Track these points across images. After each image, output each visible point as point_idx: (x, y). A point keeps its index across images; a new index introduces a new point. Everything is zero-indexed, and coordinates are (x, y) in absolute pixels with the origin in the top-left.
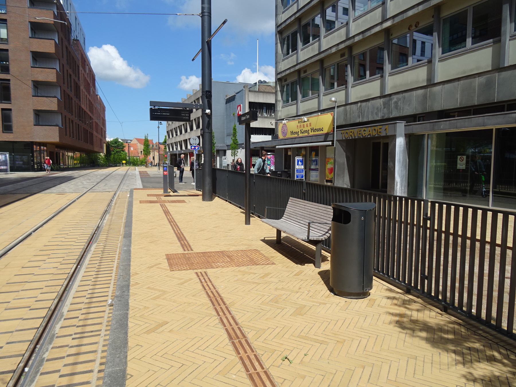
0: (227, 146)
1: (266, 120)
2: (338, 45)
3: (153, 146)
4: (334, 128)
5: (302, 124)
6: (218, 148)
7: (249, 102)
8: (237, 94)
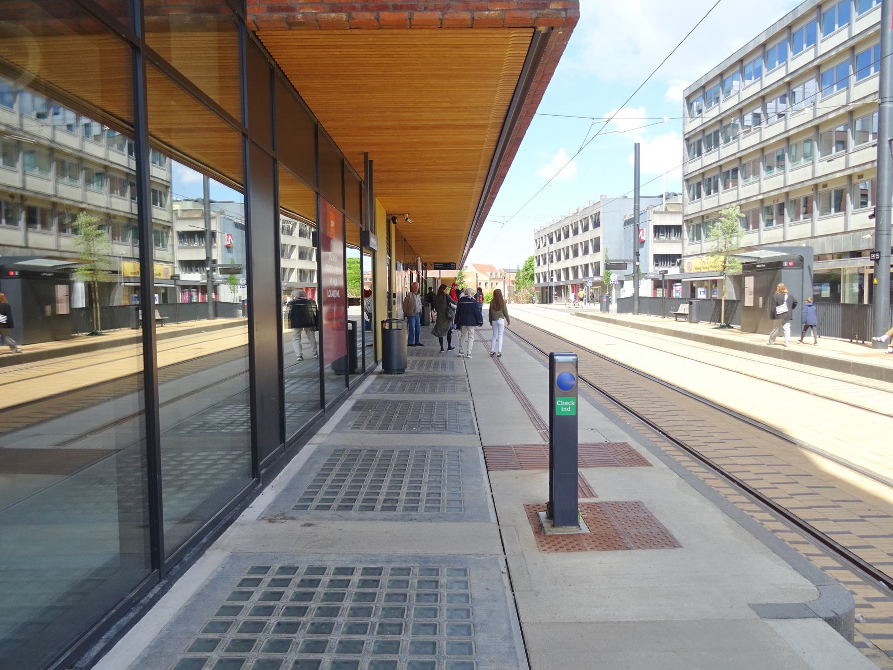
0: (625, 276)
1: (675, 244)
3: (496, 274)
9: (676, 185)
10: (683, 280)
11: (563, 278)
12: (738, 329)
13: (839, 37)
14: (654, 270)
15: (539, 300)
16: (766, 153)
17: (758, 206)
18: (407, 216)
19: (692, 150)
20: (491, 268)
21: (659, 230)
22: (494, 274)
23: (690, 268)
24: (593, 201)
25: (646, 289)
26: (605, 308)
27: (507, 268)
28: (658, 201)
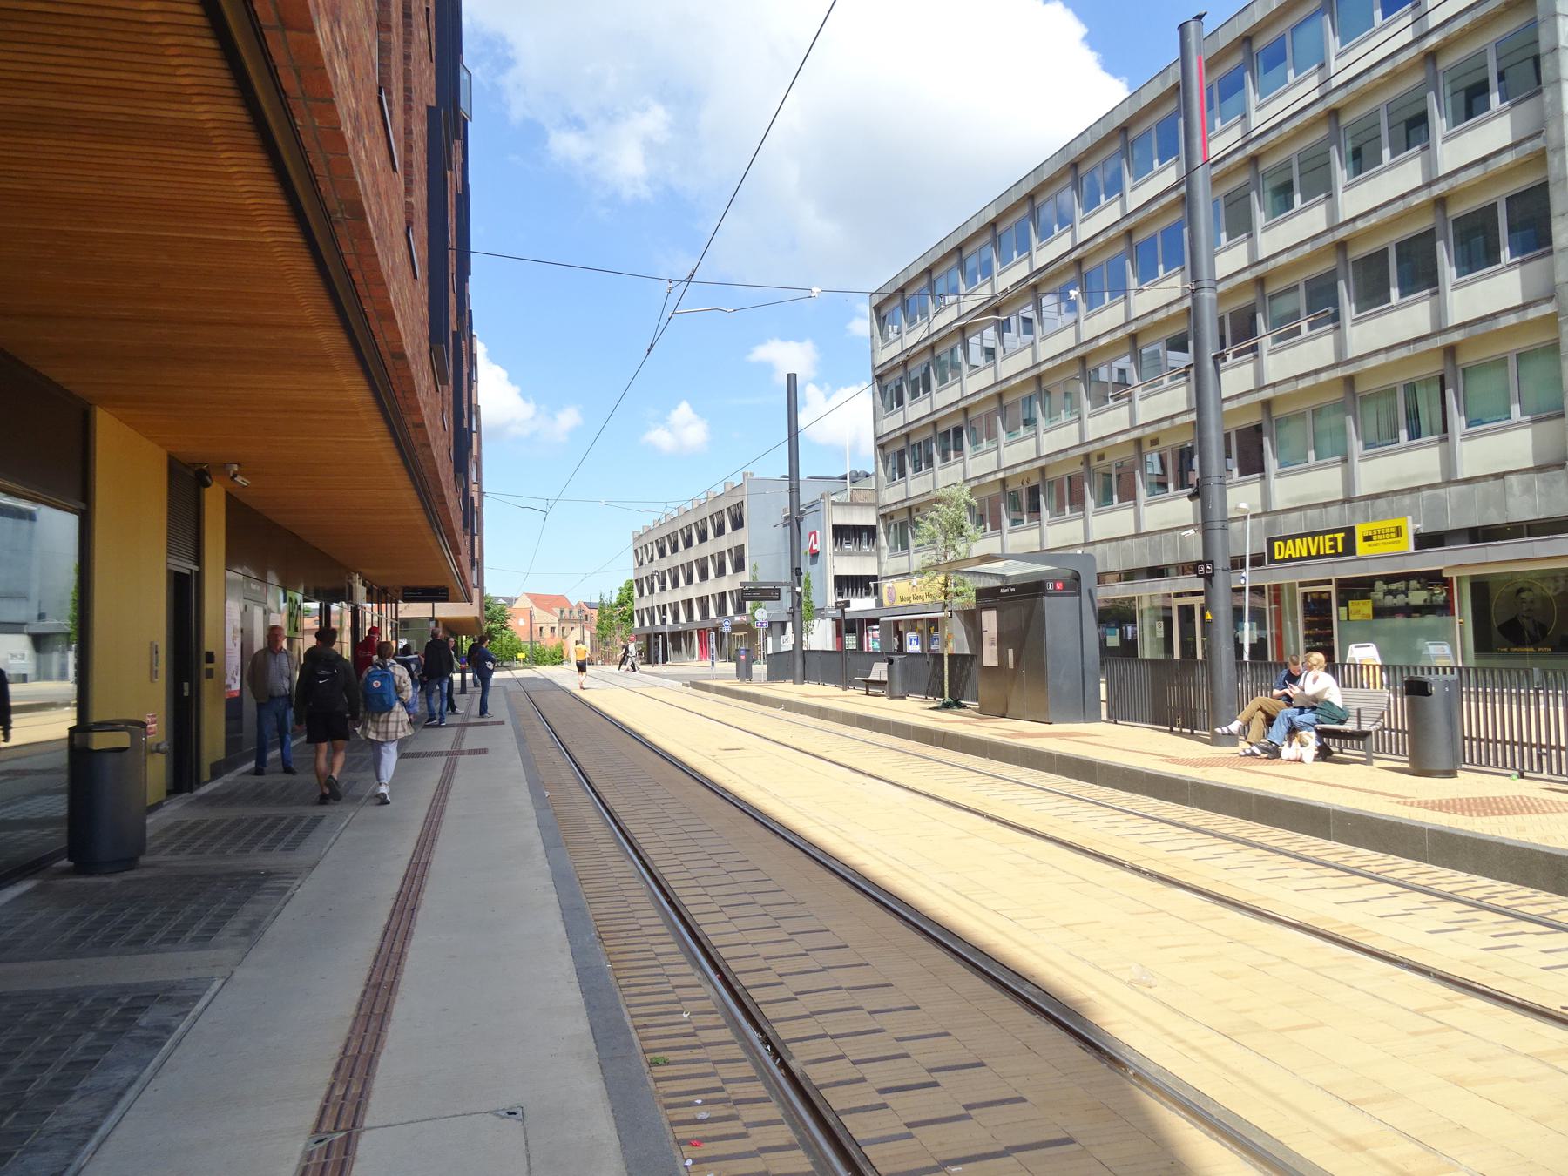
3: (571, 612)
7: (834, 527)
9: (866, 457)
10: (882, 619)
12: (974, 710)
13: (1108, 215)
16: (1006, 401)
17: (997, 490)
18: (236, 468)
19: (888, 396)
20: (560, 600)
21: (843, 534)
22: (566, 612)
23: (892, 599)
25: (821, 636)
26: (745, 673)
28: (839, 485)
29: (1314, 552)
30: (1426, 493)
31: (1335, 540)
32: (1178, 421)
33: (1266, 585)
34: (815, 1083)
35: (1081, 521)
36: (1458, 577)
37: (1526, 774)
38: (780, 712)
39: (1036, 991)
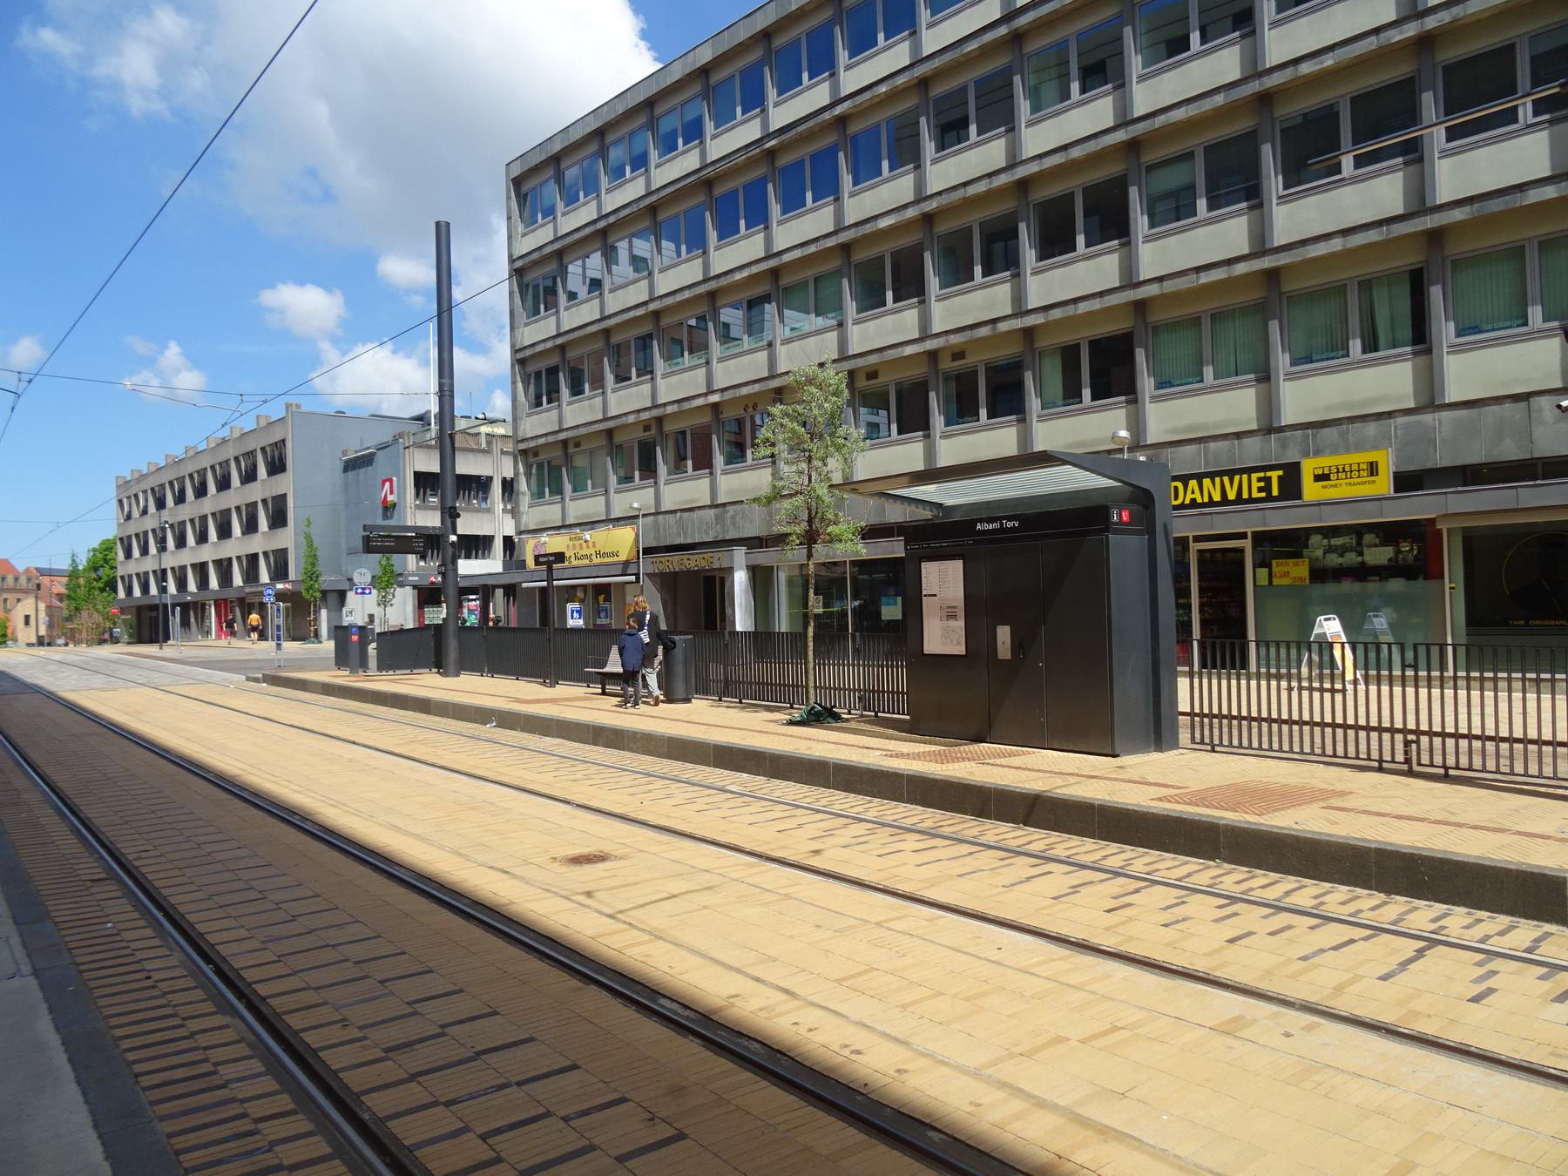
2: (638, 411)
3: (16, 579)
4: (638, 551)
5: (577, 543)
6: (325, 587)
8: (382, 451)
11: (192, 586)
14: (418, 567)
15: (130, 636)
24: (242, 429)
27: (44, 565)
29: (1232, 495)
30: (1401, 420)
31: (1268, 480)
32: (1003, 327)
33: (848, 560)
34: (407, 1143)
35: (707, 480)
36: (1448, 530)
37: (1217, 748)
38: (489, 730)
39: (692, 1015)
